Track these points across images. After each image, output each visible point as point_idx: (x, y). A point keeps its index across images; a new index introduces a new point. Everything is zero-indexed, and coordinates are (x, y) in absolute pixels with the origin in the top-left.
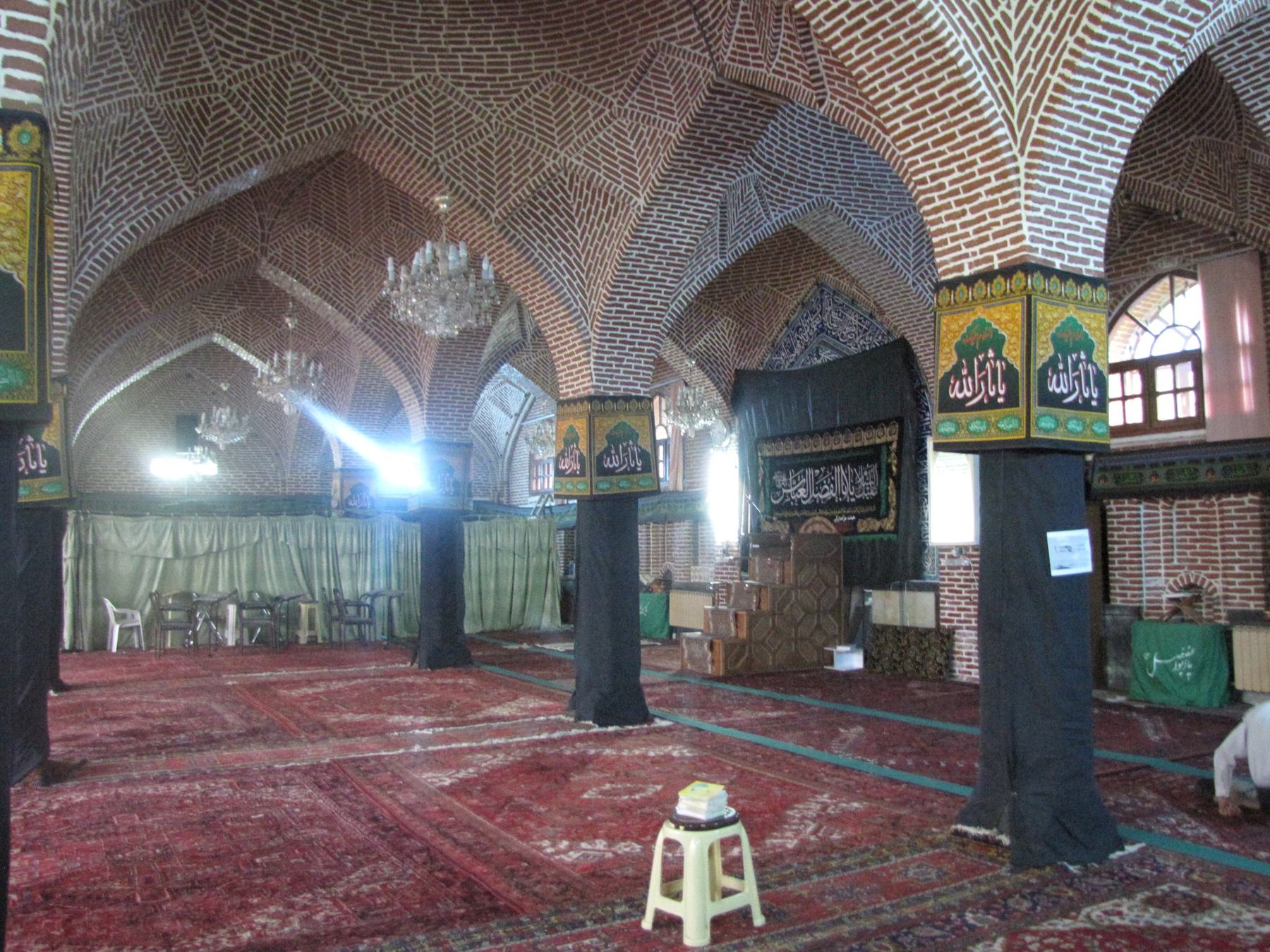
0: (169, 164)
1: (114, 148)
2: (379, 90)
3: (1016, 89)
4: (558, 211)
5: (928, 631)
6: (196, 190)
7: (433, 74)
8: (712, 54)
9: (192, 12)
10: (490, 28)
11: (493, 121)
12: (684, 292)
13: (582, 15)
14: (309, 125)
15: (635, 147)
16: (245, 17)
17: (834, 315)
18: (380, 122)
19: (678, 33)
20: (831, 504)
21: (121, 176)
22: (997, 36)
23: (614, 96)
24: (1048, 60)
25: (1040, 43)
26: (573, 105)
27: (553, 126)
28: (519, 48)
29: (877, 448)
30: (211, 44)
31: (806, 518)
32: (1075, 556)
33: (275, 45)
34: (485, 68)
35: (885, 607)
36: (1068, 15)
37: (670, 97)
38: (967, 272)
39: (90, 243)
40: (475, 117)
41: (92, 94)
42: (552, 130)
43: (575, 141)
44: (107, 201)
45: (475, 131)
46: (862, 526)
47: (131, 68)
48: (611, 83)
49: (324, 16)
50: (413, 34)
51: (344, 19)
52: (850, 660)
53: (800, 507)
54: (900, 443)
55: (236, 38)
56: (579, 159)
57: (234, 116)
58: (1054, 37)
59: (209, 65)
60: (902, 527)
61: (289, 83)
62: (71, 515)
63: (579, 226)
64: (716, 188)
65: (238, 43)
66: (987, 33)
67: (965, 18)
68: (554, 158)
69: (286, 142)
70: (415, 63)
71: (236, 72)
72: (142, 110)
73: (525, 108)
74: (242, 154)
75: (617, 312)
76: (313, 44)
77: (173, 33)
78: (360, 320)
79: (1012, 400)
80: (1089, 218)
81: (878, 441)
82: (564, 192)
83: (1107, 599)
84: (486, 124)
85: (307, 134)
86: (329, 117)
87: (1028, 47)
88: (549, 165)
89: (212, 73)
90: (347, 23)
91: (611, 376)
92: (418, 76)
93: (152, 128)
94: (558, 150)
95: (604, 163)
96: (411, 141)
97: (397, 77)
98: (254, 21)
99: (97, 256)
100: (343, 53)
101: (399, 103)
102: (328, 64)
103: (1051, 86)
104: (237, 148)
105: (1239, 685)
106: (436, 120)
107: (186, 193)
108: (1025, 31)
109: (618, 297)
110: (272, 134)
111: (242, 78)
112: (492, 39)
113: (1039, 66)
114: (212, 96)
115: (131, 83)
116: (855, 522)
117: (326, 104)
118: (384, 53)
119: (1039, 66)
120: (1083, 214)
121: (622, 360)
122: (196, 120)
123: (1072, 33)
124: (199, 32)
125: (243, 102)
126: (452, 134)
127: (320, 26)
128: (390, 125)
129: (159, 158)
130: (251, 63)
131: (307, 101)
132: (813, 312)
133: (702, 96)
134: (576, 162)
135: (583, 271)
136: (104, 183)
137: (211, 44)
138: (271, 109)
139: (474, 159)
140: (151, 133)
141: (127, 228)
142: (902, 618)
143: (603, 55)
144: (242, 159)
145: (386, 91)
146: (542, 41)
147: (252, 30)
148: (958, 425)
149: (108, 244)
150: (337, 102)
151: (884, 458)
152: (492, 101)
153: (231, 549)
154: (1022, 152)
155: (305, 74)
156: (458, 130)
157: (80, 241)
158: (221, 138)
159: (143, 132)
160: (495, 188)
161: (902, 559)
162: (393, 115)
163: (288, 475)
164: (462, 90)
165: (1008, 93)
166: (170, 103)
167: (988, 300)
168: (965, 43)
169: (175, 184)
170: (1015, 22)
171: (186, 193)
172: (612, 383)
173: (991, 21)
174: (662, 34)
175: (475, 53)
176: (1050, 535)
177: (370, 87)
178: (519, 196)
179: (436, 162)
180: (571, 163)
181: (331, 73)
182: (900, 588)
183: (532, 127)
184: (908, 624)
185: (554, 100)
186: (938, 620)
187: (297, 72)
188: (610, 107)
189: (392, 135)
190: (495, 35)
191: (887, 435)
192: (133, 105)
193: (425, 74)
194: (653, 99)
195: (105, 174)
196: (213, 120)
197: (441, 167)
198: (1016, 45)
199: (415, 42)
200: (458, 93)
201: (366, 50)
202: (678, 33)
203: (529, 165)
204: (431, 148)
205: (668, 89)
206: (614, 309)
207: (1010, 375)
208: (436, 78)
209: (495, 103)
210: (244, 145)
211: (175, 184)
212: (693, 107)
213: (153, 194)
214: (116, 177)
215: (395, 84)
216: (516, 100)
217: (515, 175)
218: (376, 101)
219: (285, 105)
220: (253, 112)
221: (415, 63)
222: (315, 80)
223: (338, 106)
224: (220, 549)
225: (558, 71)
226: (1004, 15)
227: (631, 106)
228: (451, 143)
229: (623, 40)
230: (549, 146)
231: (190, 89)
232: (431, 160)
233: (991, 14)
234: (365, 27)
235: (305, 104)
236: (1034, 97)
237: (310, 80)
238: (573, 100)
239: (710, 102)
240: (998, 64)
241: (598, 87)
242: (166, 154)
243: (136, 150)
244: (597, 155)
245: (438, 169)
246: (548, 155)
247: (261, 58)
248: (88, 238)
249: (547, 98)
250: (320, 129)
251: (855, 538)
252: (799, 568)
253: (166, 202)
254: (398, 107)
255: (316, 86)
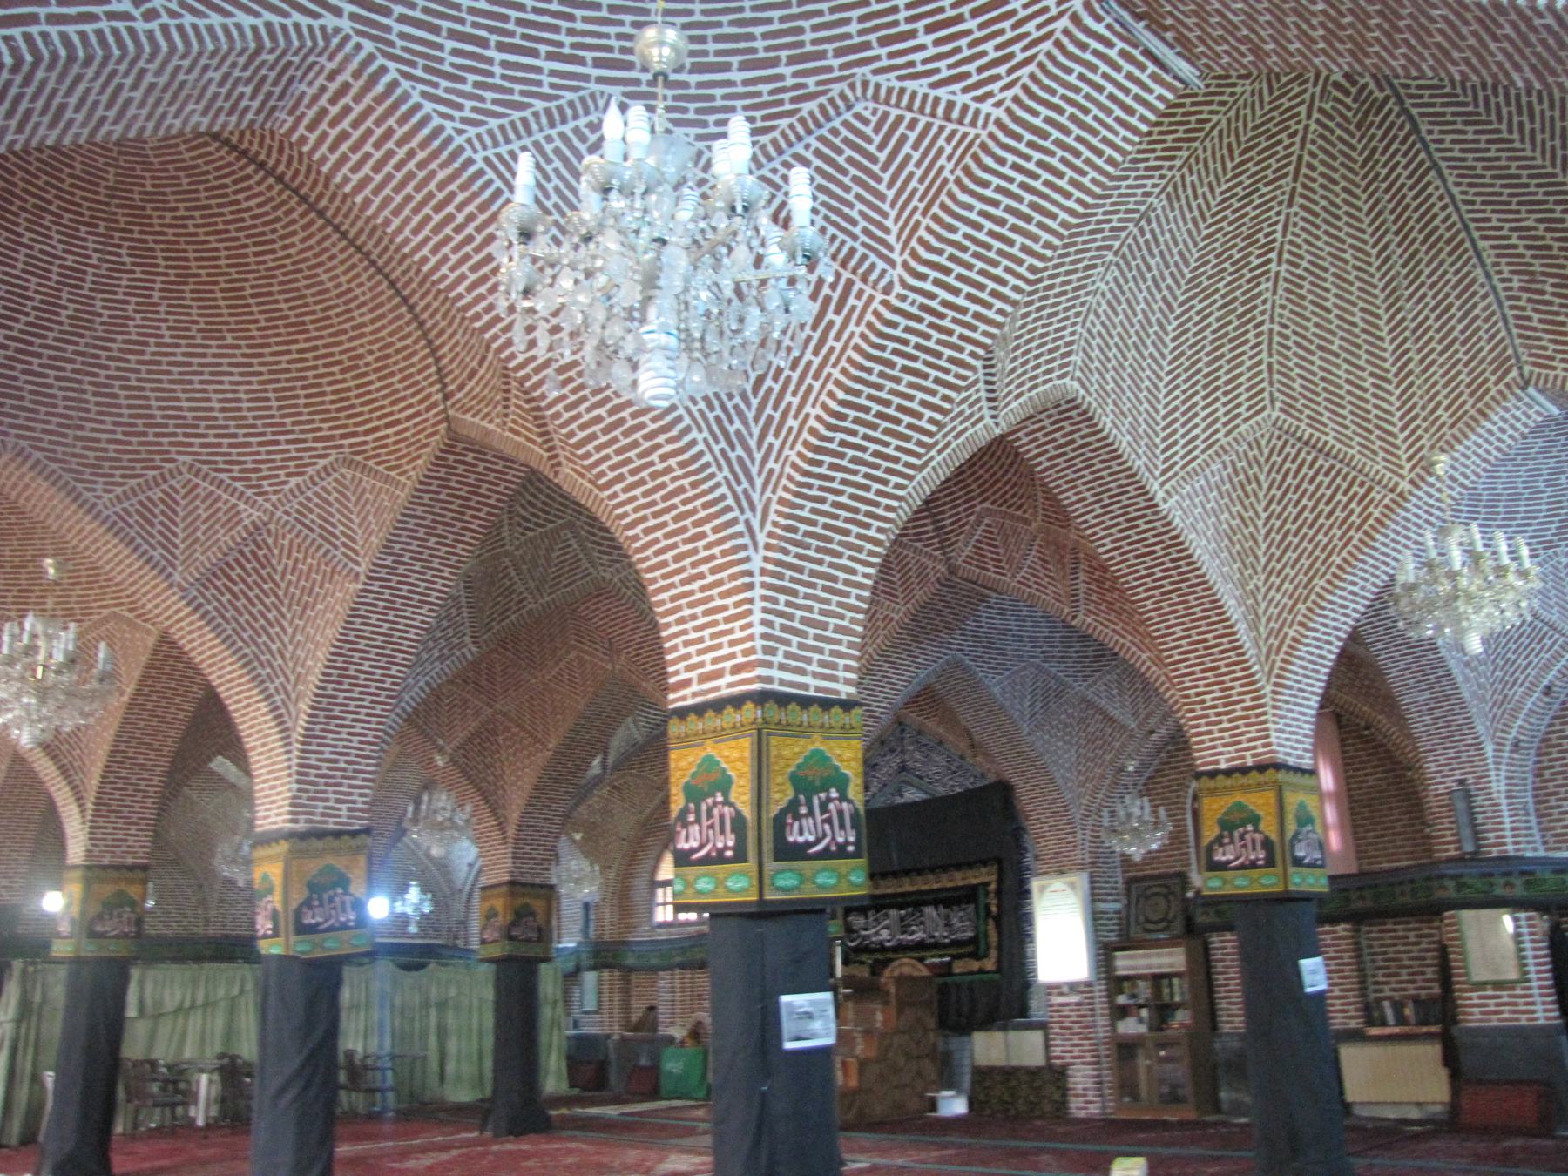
5: (1039, 1069)
17: (917, 755)
20: (920, 946)
29: (974, 888)
31: (890, 960)
32: (817, 1025)
35: (988, 1048)
38: (1223, 766)
46: (959, 967)
52: (954, 1105)
53: (882, 948)
54: (1000, 881)
60: (1005, 965)
62: (17, 964)
79: (1270, 862)
81: (975, 881)
83: (1215, 1028)
105: (1349, 1098)
116: (949, 964)
132: (892, 751)
133: (932, 587)
142: (1008, 1057)
148: (1225, 882)
151: (982, 899)
153: (206, 1005)
161: (1007, 994)
163: (212, 913)
167: (1245, 788)
176: (785, 999)
182: (1004, 1028)
184: (1015, 1063)
186: (1048, 1058)
191: (984, 876)
207: (1267, 844)
212: (920, 595)
224: (192, 1007)
251: (949, 979)
252: (900, 1012)
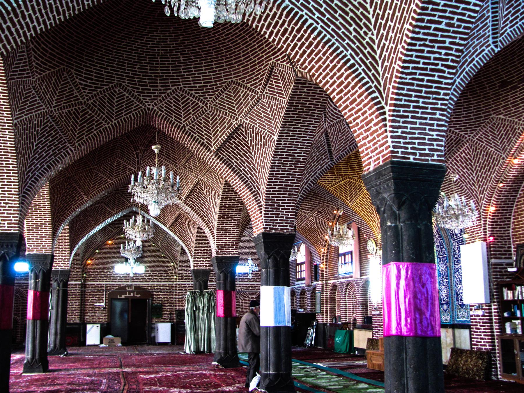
0: (62, 138)
1: (38, 133)
2: (157, 96)
3: (381, 73)
4: (242, 145)
6: (75, 148)
7: (180, 87)
8: (291, 64)
9: (68, 73)
10: (202, 63)
11: (208, 105)
12: (311, 179)
13: (240, 53)
14: (125, 115)
15: (270, 112)
16: (92, 72)
18: (157, 110)
19: (280, 57)
21: (42, 144)
22: (369, 49)
23: (259, 89)
24: (393, 57)
25: (389, 50)
26: (242, 95)
27: (234, 105)
28: (216, 71)
30: (77, 85)
33: (106, 82)
34: (202, 81)
36: (398, 35)
37: (281, 87)
39: (30, 174)
40: (200, 104)
41: (23, 113)
42: (234, 107)
43: (244, 111)
44: (37, 155)
45: (201, 111)
47: (41, 100)
48: (256, 83)
49: (128, 67)
50: (169, 70)
51: (137, 67)
55: (89, 81)
56: (247, 119)
57: (91, 114)
58: (394, 46)
59: (77, 94)
61: (115, 98)
63: (253, 151)
64: (311, 128)
65: (90, 83)
66: (363, 48)
67: (350, 43)
68: (236, 120)
69: (115, 123)
70: (171, 82)
71: (90, 95)
72: (48, 116)
73: (221, 98)
74: (95, 130)
75: (273, 191)
76: (125, 79)
77: (60, 83)
78: (184, 199)
80: (431, 133)
82: (243, 135)
84: (205, 107)
85: (124, 119)
86: (134, 110)
87: (384, 53)
88: (234, 123)
89: (79, 97)
90: (138, 68)
91: (273, 223)
92: (173, 88)
93: (53, 123)
94: (237, 116)
95: (258, 121)
96: (172, 118)
97: (163, 90)
98: (96, 73)
99: (33, 179)
100: (138, 81)
101: (166, 101)
102: (132, 87)
103: (395, 70)
104: (93, 128)
106: (183, 107)
107: (70, 149)
108: (382, 45)
109: (272, 184)
110: (109, 121)
111: (93, 98)
112: (204, 68)
113: (390, 61)
114: (80, 107)
115: (42, 106)
117: (133, 105)
118: (179, 79)
119: (390, 61)
120: (427, 131)
121: (279, 214)
122: (73, 118)
123: (400, 44)
124: (72, 81)
125: (94, 108)
126: (190, 113)
127: (127, 71)
128: (163, 112)
129: (58, 135)
130: (96, 91)
131: (124, 104)
134: (246, 121)
135: (256, 172)
136: (35, 148)
137: (77, 85)
138: (107, 109)
139: (201, 124)
140: (53, 125)
141: (45, 166)
143: (251, 71)
144: (95, 132)
145: (160, 96)
146: (225, 67)
147: (95, 77)
149: (37, 173)
150: (138, 103)
152: (207, 96)
154: (386, 104)
155: (122, 92)
156: (193, 111)
157: (25, 173)
158: (85, 124)
159: (49, 125)
160: (212, 136)
162: (163, 106)
164: (193, 92)
165: (377, 76)
166: (60, 112)
168: (351, 54)
169: (66, 146)
170: (377, 42)
171: (70, 149)
172: (273, 226)
173: (364, 42)
174: (274, 58)
175: (197, 75)
177: (152, 95)
178: (222, 139)
179: (184, 126)
180: (244, 122)
181: (134, 91)
183: (225, 106)
185: (233, 94)
187: (118, 92)
188: (257, 94)
189: (164, 115)
190: (205, 66)
192: (43, 115)
193: (176, 87)
194: (275, 89)
195: (35, 144)
196: (81, 117)
197: (187, 128)
198: (378, 52)
199: (170, 73)
200: (192, 94)
201: (148, 79)
202: (280, 57)
203: (226, 124)
204: (181, 120)
205: (280, 83)
206: (271, 190)
208: (181, 88)
209: (208, 97)
210: (96, 126)
211: (66, 146)
212: (290, 91)
213: (56, 151)
214: (40, 145)
215: (164, 93)
216: (217, 95)
217: (220, 130)
218: (155, 101)
219: (114, 107)
220: (99, 112)
221: (171, 82)
222: (127, 95)
223: (138, 105)
225: (234, 79)
226: (370, 38)
227: (266, 93)
228: (191, 117)
229: (259, 63)
230: (233, 115)
231: (69, 105)
232: (182, 125)
233: (364, 39)
234: (147, 69)
235: (123, 106)
236: (389, 76)
237: (125, 95)
238: (242, 93)
239: (295, 89)
240: (370, 62)
241: (251, 85)
242: (60, 133)
243: (47, 133)
244: (255, 117)
245: (185, 129)
246: (233, 119)
247: (101, 88)
248: (29, 172)
249: (231, 93)
250: (130, 116)
253: (62, 154)
254: (165, 103)
255: (127, 97)
